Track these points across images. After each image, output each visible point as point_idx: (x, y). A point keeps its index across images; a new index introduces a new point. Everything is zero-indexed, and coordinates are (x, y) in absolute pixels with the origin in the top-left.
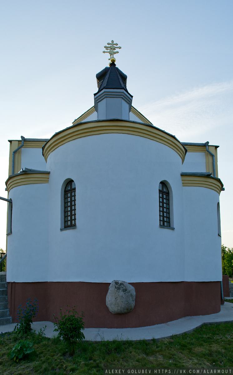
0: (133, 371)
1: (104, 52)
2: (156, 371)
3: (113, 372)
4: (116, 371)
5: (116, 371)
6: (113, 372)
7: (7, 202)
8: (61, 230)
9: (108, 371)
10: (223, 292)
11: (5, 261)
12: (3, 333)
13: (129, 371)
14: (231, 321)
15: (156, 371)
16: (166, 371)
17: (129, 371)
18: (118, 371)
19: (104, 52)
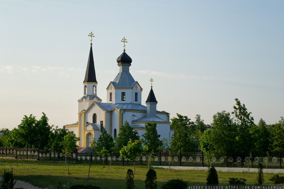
0: (256, 187)
1: (89, 36)
2: (226, 188)
3: (220, 188)
4: (197, 188)
5: (197, 188)
6: (220, 188)
7: (142, 104)
8: (262, 120)
9: (190, 187)
10: (190, 171)
11: (85, 164)
12: (245, 179)
13: (206, 187)
14: (124, 180)
15: (227, 187)
16: (235, 187)
17: (206, 187)
18: (198, 187)
19: (89, 36)
